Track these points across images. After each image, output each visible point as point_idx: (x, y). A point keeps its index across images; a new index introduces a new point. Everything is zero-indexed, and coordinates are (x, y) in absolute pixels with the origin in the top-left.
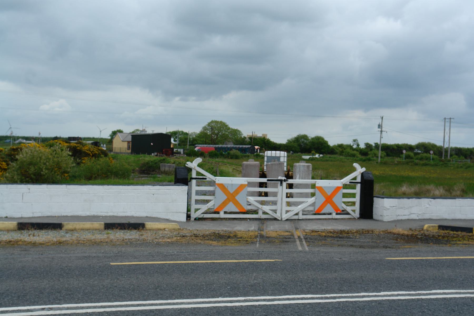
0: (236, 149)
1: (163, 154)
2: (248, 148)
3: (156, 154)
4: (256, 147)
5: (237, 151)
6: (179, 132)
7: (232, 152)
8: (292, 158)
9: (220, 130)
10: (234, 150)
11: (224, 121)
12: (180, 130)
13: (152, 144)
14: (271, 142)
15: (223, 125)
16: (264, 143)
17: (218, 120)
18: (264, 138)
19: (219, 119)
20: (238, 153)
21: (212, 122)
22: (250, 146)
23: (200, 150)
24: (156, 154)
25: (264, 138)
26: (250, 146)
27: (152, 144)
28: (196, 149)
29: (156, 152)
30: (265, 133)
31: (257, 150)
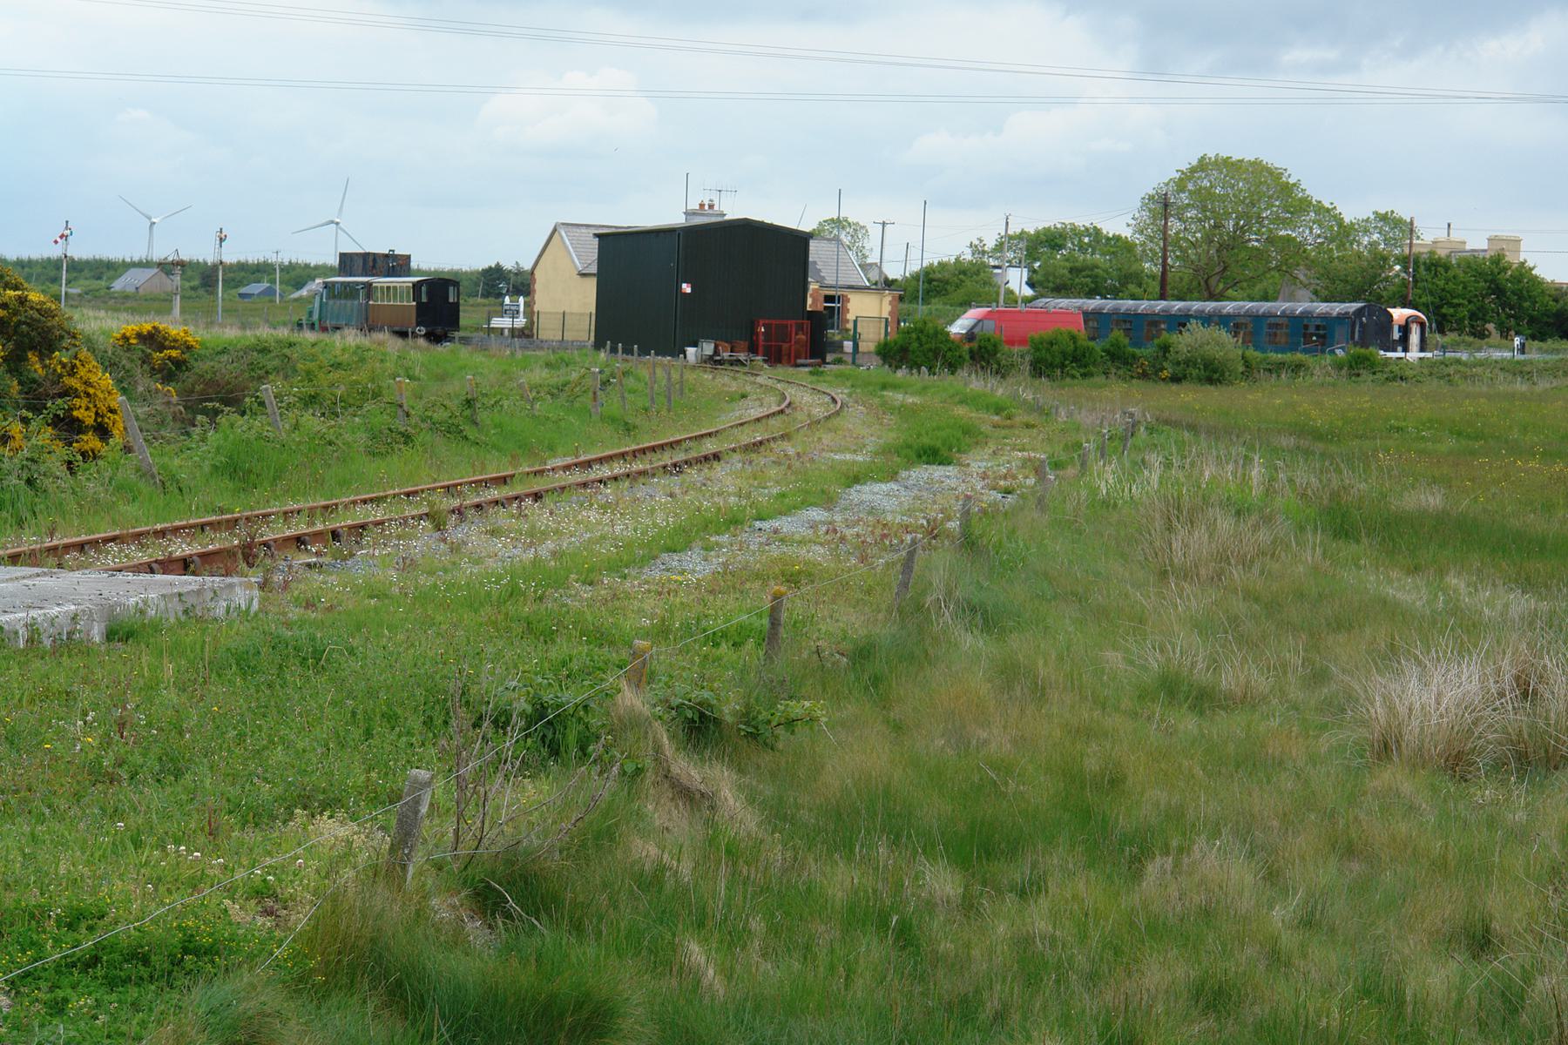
0: (1207, 319)
1: (753, 350)
2: (1342, 318)
3: (708, 348)
4: (1399, 314)
5: (1224, 336)
6: (1076, 232)
7: (1184, 342)
8: (34, 467)
9: (1250, 217)
10: (1193, 324)
11: (1272, 158)
12: (1082, 221)
13: (686, 288)
14: (1536, 282)
15: (1264, 187)
16: (1497, 290)
17: (1236, 157)
18: (1497, 260)
19: (1241, 151)
20: (1224, 344)
21: (1203, 165)
22: (1353, 307)
23: (990, 325)
24: (708, 348)
25: (1497, 260)
26: (1353, 307)
27: (686, 288)
28: (958, 328)
29: (708, 337)
30: (1506, 231)
31: (1405, 330)
